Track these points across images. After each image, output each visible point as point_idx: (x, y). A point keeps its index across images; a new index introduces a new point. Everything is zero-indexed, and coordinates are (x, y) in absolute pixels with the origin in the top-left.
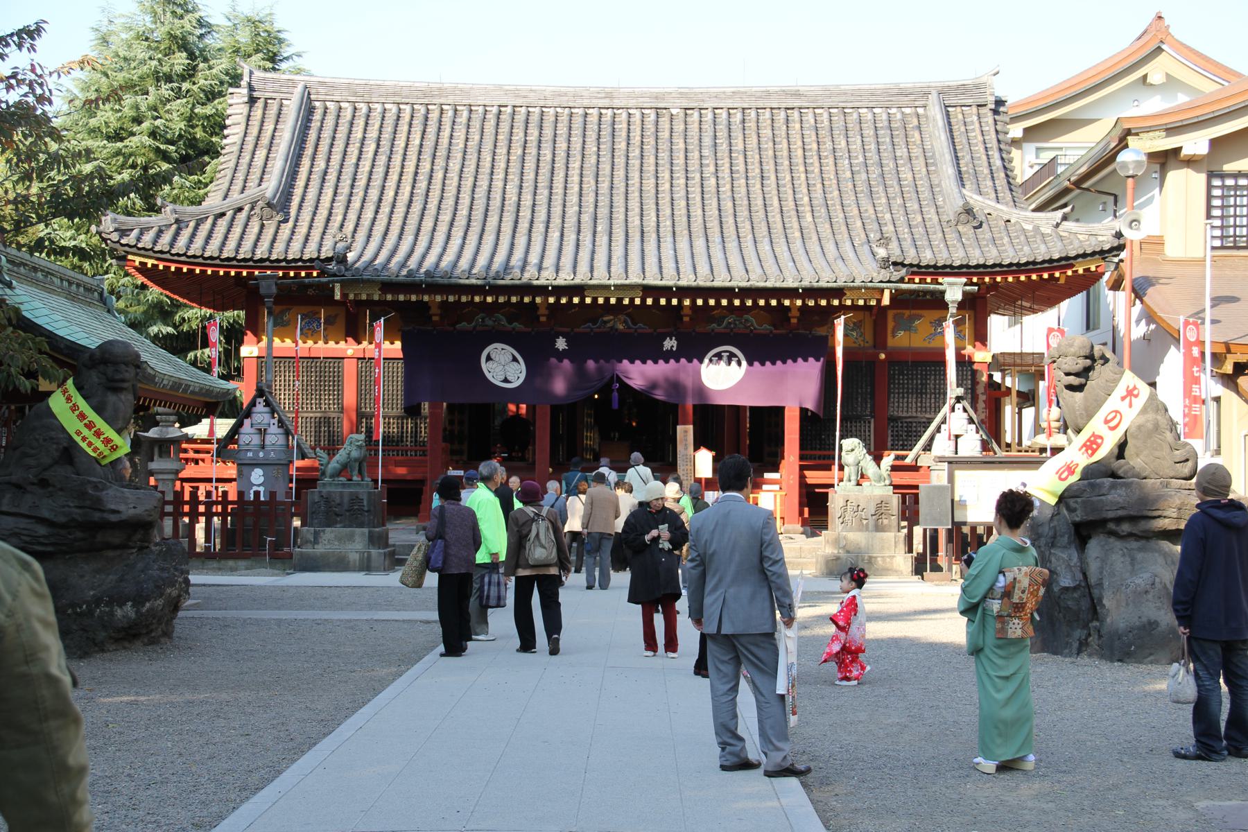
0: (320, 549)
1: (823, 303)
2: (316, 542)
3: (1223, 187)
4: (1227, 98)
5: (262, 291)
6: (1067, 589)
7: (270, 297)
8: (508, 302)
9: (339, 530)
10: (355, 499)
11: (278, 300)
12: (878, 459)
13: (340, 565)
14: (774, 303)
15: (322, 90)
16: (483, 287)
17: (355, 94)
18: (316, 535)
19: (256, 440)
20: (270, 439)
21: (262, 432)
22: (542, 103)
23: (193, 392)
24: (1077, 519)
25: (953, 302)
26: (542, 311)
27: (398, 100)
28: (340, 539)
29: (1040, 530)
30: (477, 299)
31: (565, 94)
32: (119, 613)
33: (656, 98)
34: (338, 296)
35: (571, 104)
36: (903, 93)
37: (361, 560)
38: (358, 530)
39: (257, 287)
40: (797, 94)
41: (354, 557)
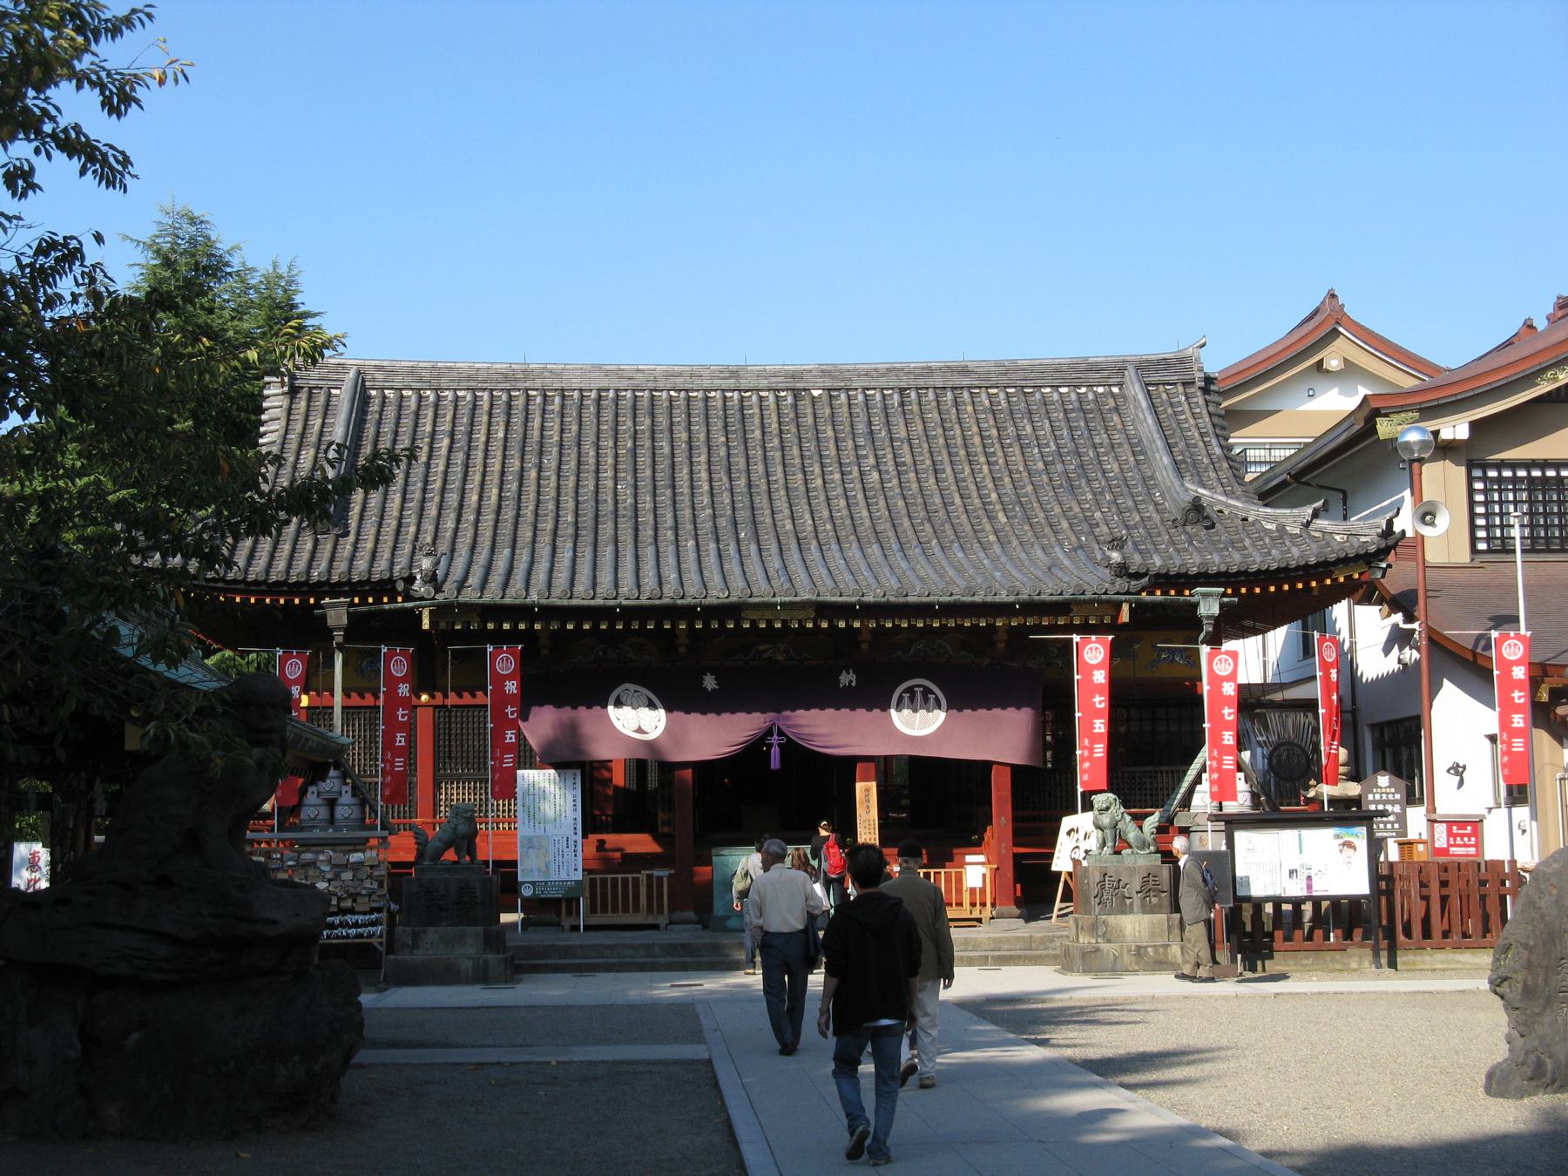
0: (420, 955)
2: (415, 945)
3: (1484, 479)
5: (331, 622)
7: (339, 629)
8: (912, 627)
11: (352, 631)
12: (1139, 819)
13: (447, 975)
15: (379, 376)
17: (420, 380)
19: (324, 813)
20: (341, 812)
21: (332, 803)
22: (651, 385)
25: (1209, 617)
27: (473, 384)
31: (680, 375)
33: (793, 377)
34: (426, 625)
35: (688, 386)
36: (1094, 368)
39: (324, 617)
40: (964, 371)
41: (466, 965)
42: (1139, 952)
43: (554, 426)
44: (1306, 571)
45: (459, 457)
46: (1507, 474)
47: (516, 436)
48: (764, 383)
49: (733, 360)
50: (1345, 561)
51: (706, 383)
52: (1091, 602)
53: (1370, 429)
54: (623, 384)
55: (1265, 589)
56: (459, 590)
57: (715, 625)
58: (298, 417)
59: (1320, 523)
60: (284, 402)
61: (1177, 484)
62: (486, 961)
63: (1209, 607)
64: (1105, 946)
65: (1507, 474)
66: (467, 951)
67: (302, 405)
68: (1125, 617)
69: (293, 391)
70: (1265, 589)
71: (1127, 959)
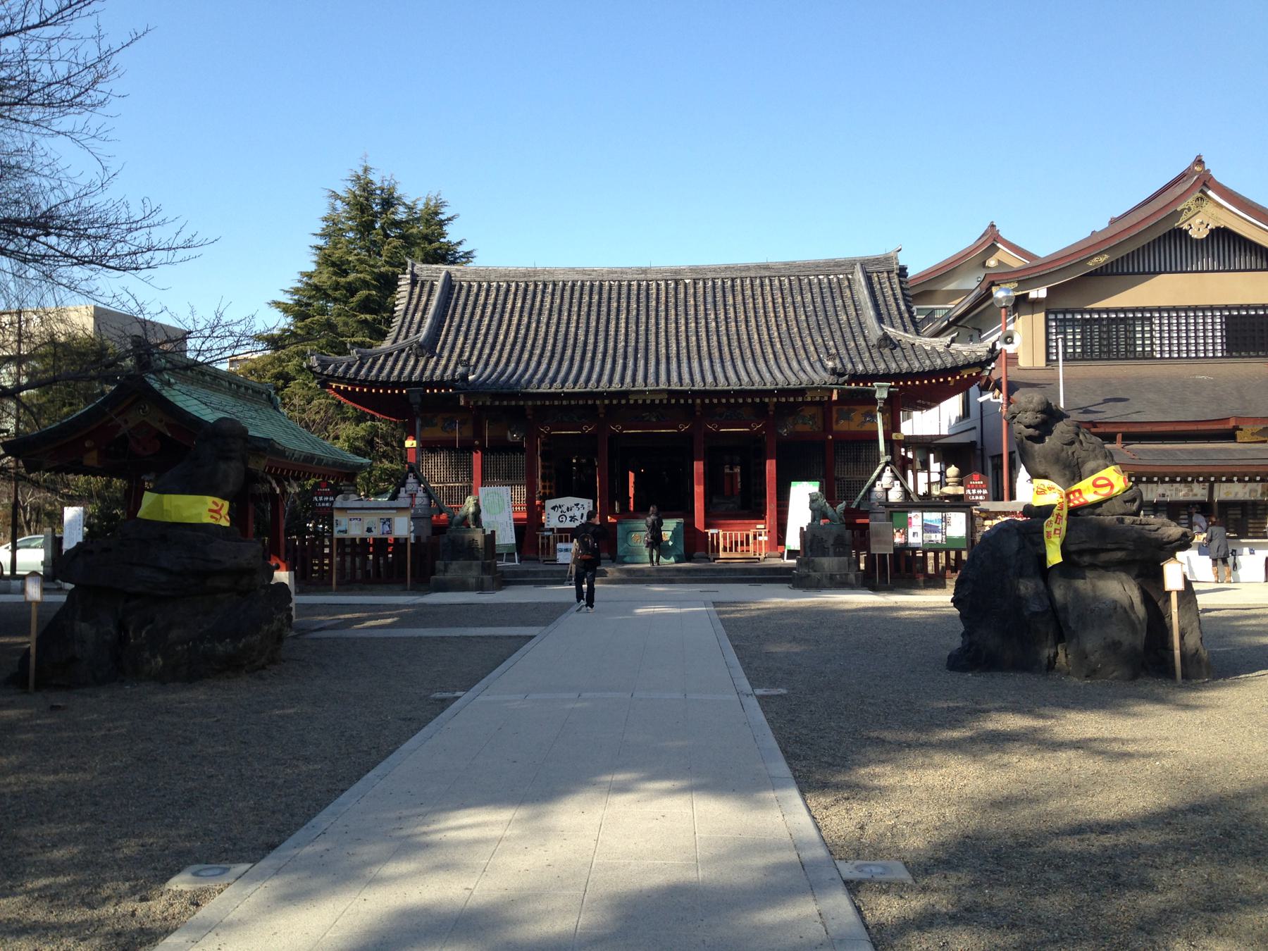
0: (449, 576)
2: (446, 571)
3: (1055, 320)
6: (1036, 613)
9: (462, 562)
13: (462, 587)
18: (446, 566)
20: (418, 501)
21: (412, 496)
23: (327, 464)
26: (601, 410)
30: (556, 403)
32: (220, 648)
34: (462, 403)
38: (475, 562)
41: (472, 581)
42: (832, 577)
43: (548, 299)
44: (945, 372)
45: (497, 316)
46: (1069, 316)
47: (527, 306)
48: (659, 276)
49: (644, 264)
50: (968, 366)
51: (629, 277)
52: (816, 388)
53: (989, 295)
54: (585, 278)
55: (432, 391)
56: (563, 386)
57: (741, 401)
58: (415, 297)
59: (954, 345)
60: (408, 288)
61: (876, 325)
63: (882, 393)
64: (813, 574)
65: (1069, 316)
66: (473, 574)
67: (417, 290)
68: (835, 397)
69: (414, 283)
70: (432, 391)
71: (825, 581)
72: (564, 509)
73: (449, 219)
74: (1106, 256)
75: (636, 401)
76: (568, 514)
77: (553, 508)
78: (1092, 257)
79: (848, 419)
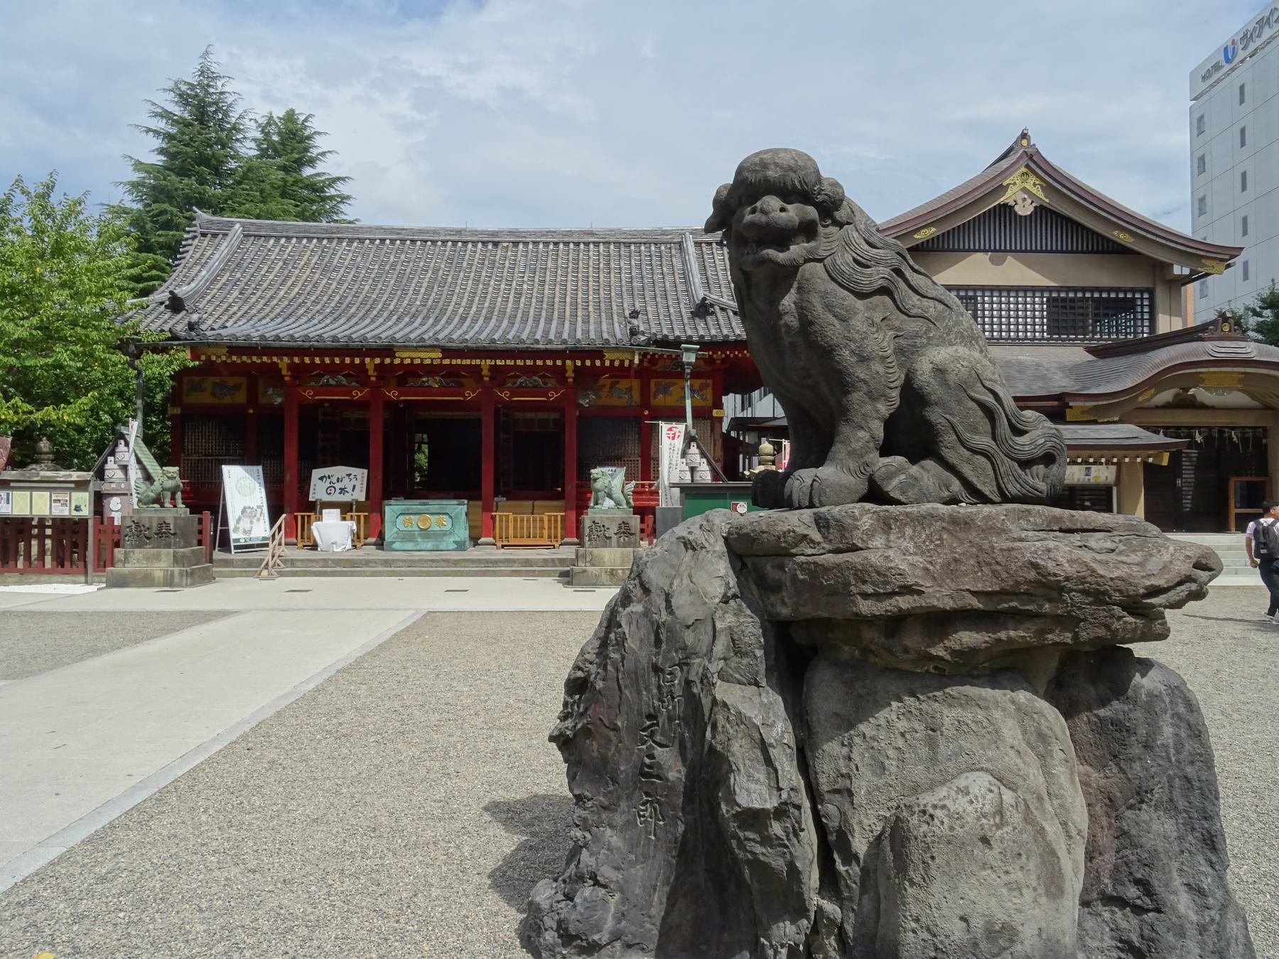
1: (337, 361)
2: (126, 560)
4: (975, 190)
9: (149, 551)
10: (163, 523)
13: (145, 581)
14: (327, 360)
16: (563, 351)
21: (125, 468)
24: (785, 611)
26: (570, 374)
28: (148, 559)
29: (689, 638)
37: (165, 577)
38: (164, 551)
40: (591, 233)
41: (159, 574)
62: (172, 572)
63: (689, 358)
71: (605, 578)
72: (334, 480)
73: (323, 154)
74: (934, 229)
75: (612, 362)
76: (338, 486)
77: (321, 479)
78: (918, 230)
79: (666, 392)
